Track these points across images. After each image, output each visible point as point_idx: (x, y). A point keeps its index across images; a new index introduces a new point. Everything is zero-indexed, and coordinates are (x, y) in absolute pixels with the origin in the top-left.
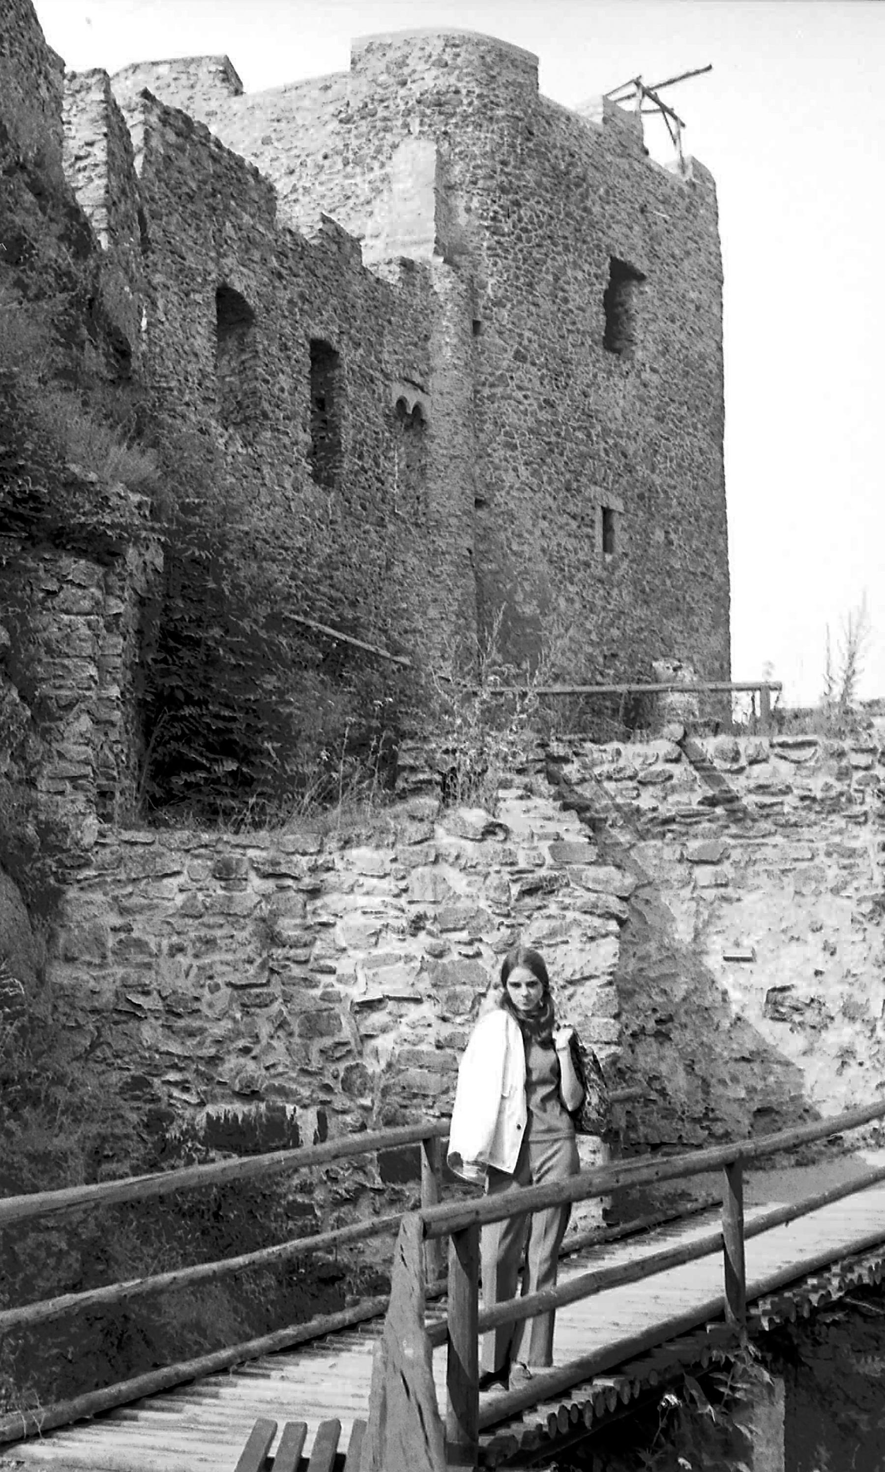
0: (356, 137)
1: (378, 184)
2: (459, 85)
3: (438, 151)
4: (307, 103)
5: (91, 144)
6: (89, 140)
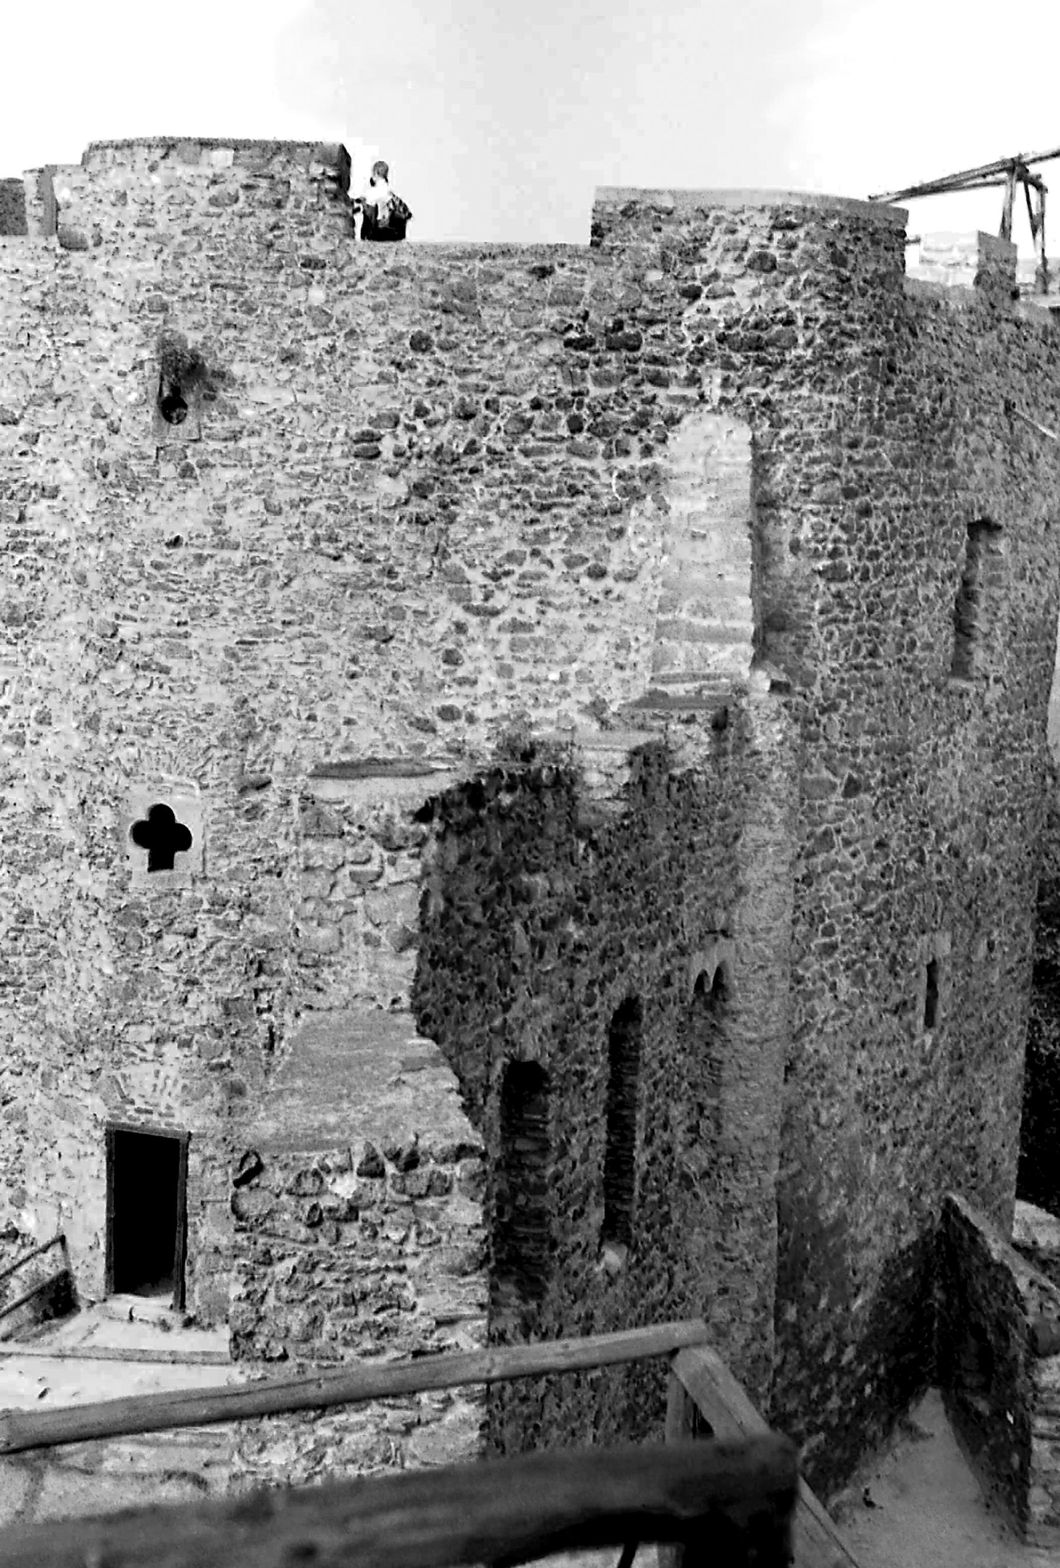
0: (598, 381)
1: (637, 482)
2: (793, 305)
3: (754, 443)
4: (500, 290)
5: (448, 1322)
6: (441, 1312)
